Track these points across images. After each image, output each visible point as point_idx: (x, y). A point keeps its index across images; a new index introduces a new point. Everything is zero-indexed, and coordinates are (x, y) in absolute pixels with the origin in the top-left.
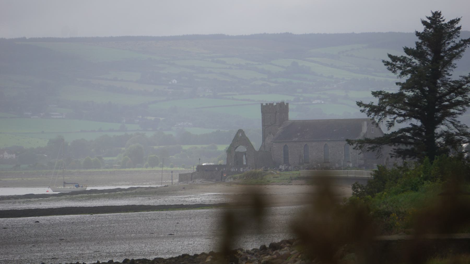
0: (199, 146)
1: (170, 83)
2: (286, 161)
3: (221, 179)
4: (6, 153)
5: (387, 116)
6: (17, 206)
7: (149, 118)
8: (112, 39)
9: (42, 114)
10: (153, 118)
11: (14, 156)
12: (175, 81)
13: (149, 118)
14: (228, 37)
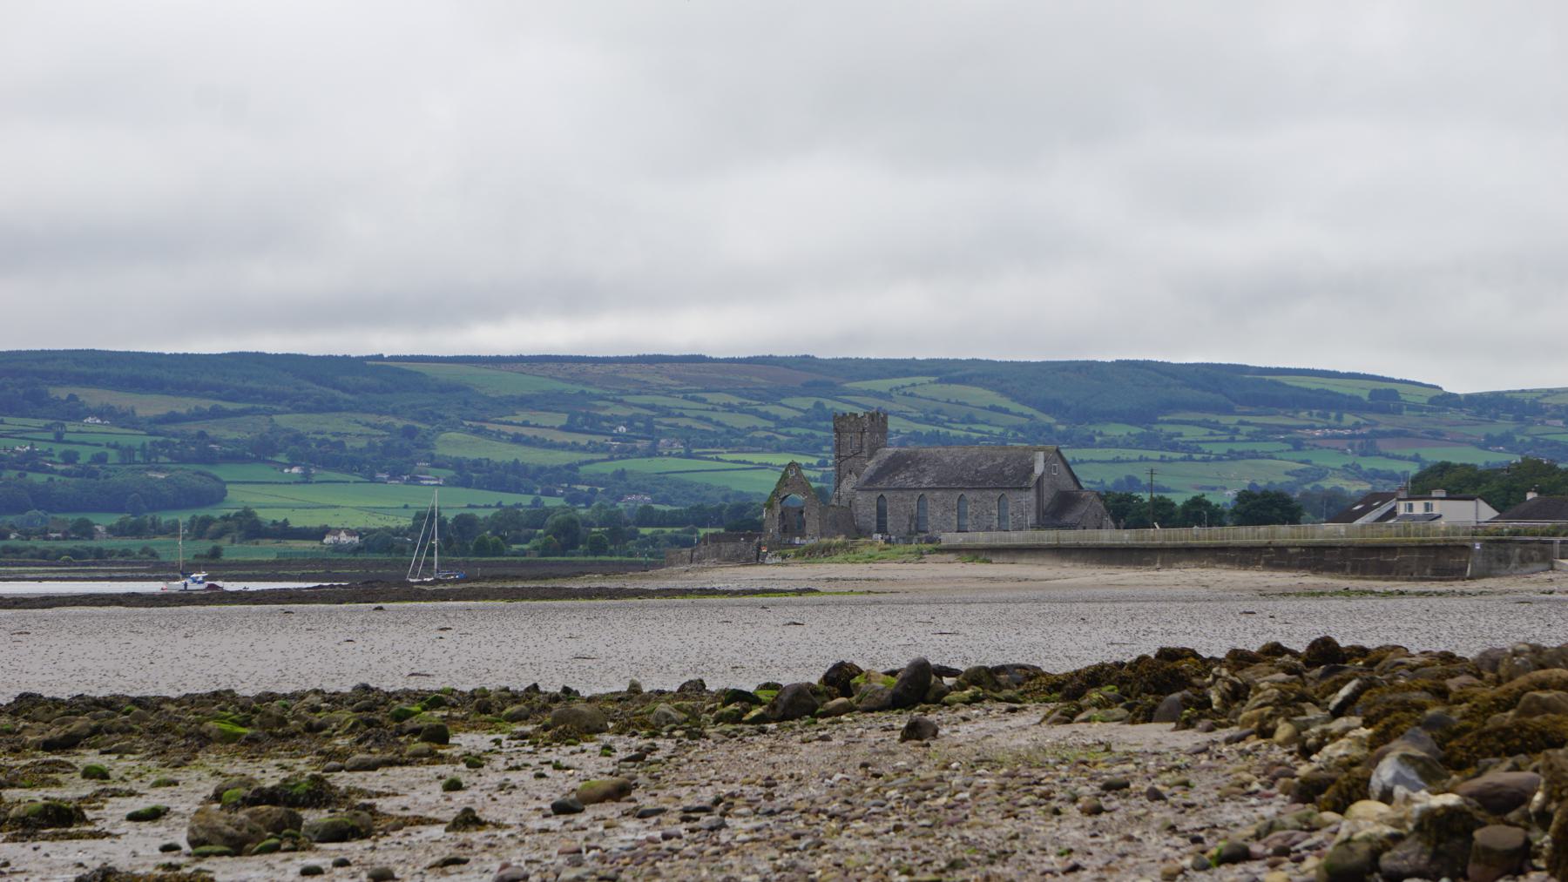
0: (668, 530)
1: (615, 432)
2: (882, 528)
3: (757, 559)
4: (343, 534)
5: (343, 788)
6: (373, 767)
7: (580, 487)
8: (521, 359)
9: (405, 478)
10: (586, 488)
11: (357, 539)
12: (622, 429)
13: (580, 487)
14: (711, 360)
